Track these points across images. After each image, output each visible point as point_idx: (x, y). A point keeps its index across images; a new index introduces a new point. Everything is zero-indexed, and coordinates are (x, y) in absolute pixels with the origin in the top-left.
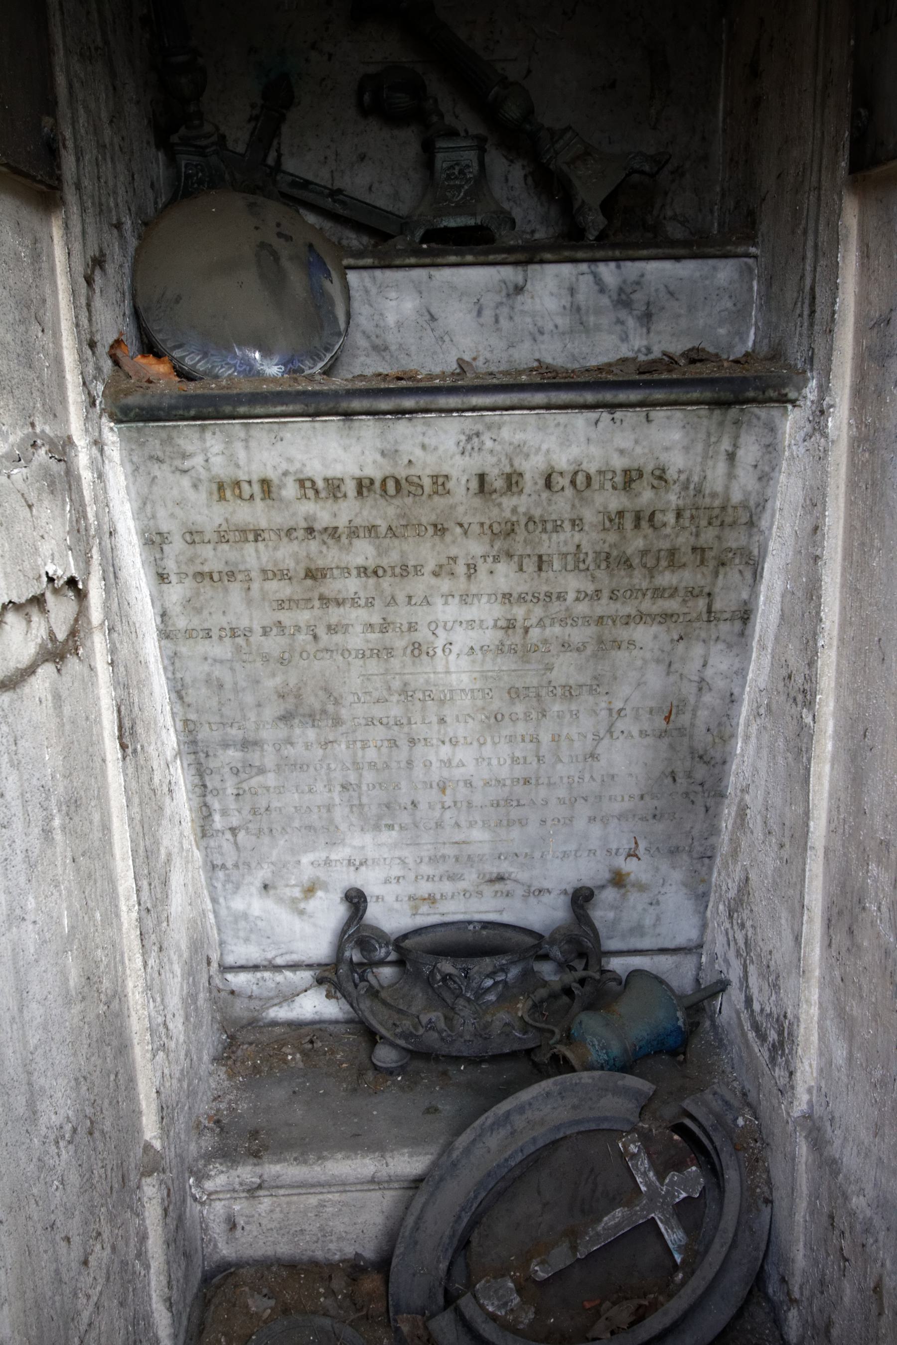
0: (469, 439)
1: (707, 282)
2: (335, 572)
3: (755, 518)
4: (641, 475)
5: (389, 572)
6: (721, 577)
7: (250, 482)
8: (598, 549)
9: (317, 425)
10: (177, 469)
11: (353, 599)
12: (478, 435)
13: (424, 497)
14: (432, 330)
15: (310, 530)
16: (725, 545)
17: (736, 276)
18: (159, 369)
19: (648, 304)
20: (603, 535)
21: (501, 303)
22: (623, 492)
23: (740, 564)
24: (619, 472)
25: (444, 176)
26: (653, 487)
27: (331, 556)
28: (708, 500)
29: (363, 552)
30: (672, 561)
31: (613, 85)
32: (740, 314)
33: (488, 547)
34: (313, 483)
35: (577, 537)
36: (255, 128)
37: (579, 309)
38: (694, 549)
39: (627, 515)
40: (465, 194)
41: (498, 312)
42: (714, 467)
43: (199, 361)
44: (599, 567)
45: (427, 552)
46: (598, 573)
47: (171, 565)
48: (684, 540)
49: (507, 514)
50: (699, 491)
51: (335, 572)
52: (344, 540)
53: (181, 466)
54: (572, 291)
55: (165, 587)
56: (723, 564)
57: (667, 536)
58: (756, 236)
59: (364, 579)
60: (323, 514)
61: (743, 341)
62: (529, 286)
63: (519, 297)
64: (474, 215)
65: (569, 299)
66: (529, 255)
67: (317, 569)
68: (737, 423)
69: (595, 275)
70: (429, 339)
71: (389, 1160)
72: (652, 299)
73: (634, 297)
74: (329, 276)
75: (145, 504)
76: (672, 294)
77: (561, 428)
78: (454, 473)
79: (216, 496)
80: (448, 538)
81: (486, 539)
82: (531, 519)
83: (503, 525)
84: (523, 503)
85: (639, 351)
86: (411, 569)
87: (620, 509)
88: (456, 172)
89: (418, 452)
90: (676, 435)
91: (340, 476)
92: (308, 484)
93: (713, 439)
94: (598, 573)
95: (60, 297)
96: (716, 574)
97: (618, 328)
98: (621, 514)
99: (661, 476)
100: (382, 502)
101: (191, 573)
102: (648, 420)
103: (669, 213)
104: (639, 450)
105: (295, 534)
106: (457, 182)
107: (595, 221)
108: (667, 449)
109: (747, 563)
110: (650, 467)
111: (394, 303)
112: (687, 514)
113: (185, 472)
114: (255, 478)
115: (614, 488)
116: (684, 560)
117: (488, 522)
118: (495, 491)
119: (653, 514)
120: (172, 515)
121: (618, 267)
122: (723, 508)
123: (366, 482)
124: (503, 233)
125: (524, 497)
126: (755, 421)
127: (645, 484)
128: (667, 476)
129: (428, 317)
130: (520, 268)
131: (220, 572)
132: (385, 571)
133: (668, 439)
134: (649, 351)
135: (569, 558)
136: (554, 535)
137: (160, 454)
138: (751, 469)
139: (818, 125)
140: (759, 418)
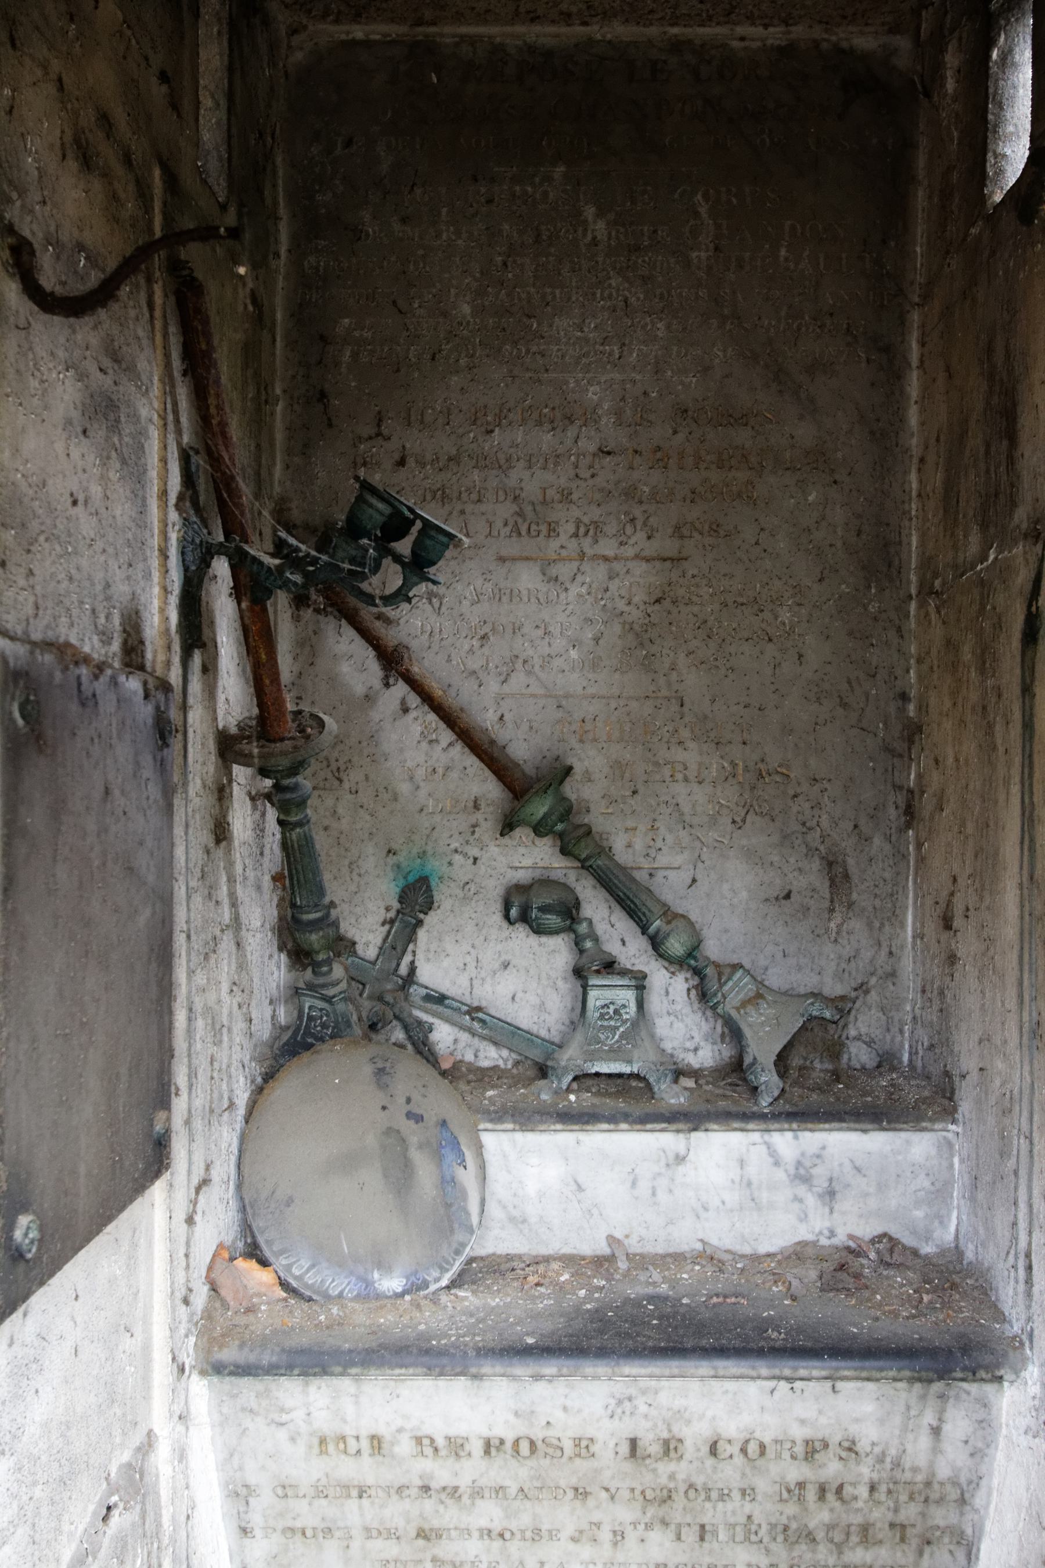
0: (620, 1402)
1: (900, 1158)
2: (453, 1533)
3: (967, 1496)
5: (518, 1536)
6: (926, 1556)
7: (357, 1438)
8: (773, 1521)
10: (273, 1421)
11: (473, 1562)
13: (565, 1459)
14: (579, 1202)
15: (426, 1489)
18: (258, 1278)
19: (831, 1180)
20: (780, 1507)
21: (659, 1174)
22: (804, 1463)
23: (951, 1543)
24: (799, 1442)
25: (597, 1015)
26: (841, 1458)
27: (449, 1516)
28: (908, 1476)
29: (489, 1513)
30: (866, 1536)
31: (788, 896)
33: (639, 1513)
34: (432, 1440)
35: (748, 1508)
36: (389, 932)
37: (749, 1184)
38: (892, 1525)
39: (809, 1486)
40: (621, 1037)
42: (915, 1440)
43: (308, 1270)
44: (775, 1539)
45: (566, 1517)
46: (773, 1546)
47: (256, 1519)
48: (880, 1515)
49: (663, 1480)
50: (897, 1464)
51: (453, 1533)
52: (465, 1499)
53: (277, 1419)
55: (247, 1542)
56: (929, 1543)
57: (858, 1510)
58: (955, 1110)
59: (487, 1542)
60: (442, 1472)
63: (680, 1168)
64: (629, 1062)
66: (690, 1119)
67: (431, 1530)
71: (491, 809)
72: (835, 1175)
74: (461, 1155)
75: (232, 1455)
76: (858, 1170)
78: (600, 1436)
79: (316, 1450)
80: (591, 1502)
81: (638, 1505)
82: (691, 1486)
83: (658, 1492)
84: (683, 1470)
85: (821, 1233)
86: (545, 1534)
87: (801, 1479)
88: (611, 1011)
90: (869, 1408)
91: (465, 1435)
92: (426, 1442)
93: (913, 1413)
94: (773, 1546)
95: (156, 1266)
96: (921, 1553)
97: (796, 1206)
98: (801, 1485)
99: (851, 1448)
100: (513, 1462)
101: (280, 1527)
103: (853, 1033)
104: (823, 1420)
105: (407, 1492)
106: (612, 1023)
107: (768, 1079)
109: (958, 1543)
110: (837, 1438)
112: (883, 1488)
113: (282, 1424)
114: (364, 1433)
115: (793, 1457)
116: (880, 1536)
117: (639, 1488)
118: (649, 1456)
120: (263, 1467)
121: (796, 1138)
122: (928, 1484)
123: (495, 1442)
124: (663, 1087)
125: (683, 1464)
126: (964, 1396)
127: (831, 1455)
128: (858, 1448)
129: (575, 1187)
130: (681, 1136)
131: (314, 1529)
132: (513, 1534)
133: (861, 1410)
134: (832, 1234)
135: (738, 1529)
136: (720, 1505)
137: (255, 1406)
138: (961, 1445)
139: (1027, 1068)
140: (968, 1393)
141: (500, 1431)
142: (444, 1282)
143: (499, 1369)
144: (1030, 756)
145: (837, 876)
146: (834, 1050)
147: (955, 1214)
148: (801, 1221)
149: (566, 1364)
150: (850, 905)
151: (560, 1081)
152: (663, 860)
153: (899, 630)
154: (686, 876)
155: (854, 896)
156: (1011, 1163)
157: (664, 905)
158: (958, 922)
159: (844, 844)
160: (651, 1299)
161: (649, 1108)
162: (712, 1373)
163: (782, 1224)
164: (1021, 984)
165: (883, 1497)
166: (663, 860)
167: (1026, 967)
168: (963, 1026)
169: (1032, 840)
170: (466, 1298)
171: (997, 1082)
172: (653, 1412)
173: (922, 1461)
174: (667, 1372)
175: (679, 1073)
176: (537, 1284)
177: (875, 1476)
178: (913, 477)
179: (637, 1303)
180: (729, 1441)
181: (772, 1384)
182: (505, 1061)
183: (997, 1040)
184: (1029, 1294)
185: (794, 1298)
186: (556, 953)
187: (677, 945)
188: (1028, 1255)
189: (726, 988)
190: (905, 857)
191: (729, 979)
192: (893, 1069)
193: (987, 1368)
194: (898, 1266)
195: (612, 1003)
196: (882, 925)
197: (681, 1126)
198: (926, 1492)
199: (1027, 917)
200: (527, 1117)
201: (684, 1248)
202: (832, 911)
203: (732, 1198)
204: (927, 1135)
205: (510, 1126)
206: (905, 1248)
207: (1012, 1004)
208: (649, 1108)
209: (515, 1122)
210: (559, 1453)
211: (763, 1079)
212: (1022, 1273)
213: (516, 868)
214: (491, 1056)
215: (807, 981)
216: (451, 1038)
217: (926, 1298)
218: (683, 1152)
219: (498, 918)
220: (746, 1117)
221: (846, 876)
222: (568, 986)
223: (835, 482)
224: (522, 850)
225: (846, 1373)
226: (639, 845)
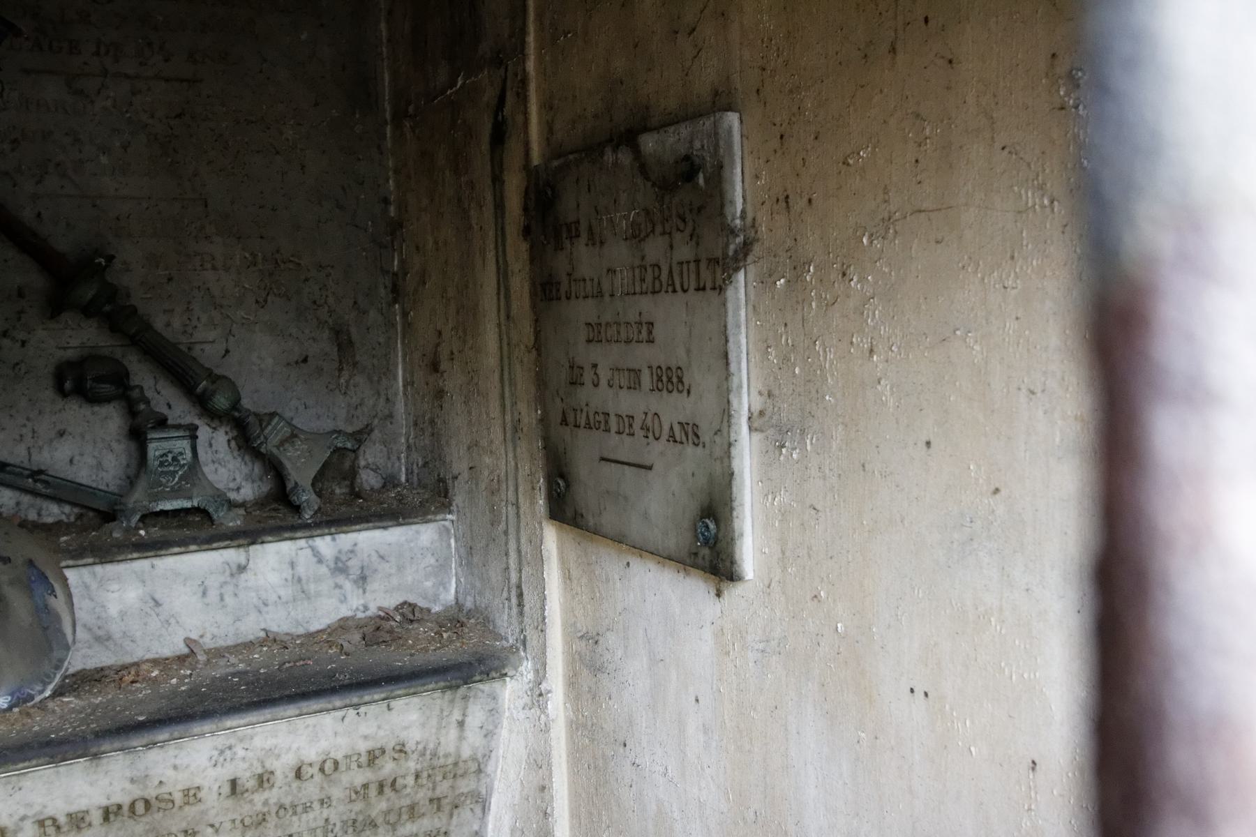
0: (222, 752)
4: (384, 752)
8: (345, 818)
9: (61, 769)
12: (230, 748)
16: (457, 792)
17: (436, 537)
19: (362, 568)
20: (350, 806)
21: (225, 583)
24: (363, 754)
25: (157, 463)
28: (442, 761)
31: (305, 360)
32: (442, 567)
34: (54, 820)
35: (326, 813)
37: (300, 580)
38: (431, 800)
40: (181, 479)
41: (223, 591)
49: (259, 807)
50: (434, 755)
54: (292, 565)
57: (408, 795)
58: (451, 504)
61: (446, 589)
62: (251, 565)
64: (190, 498)
65: (290, 572)
66: (250, 536)
68: (465, 698)
69: (312, 548)
70: (154, 623)
73: (350, 563)
76: (382, 557)
77: (311, 729)
82: (282, 807)
84: (273, 795)
85: (357, 609)
89: (170, 773)
92: (49, 823)
93: (445, 713)
96: (451, 815)
97: (337, 591)
98: (366, 786)
99: (401, 750)
100: (131, 822)
102: (389, 708)
104: (381, 733)
106: (172, 468)
107: (307, 497)
108: (406, 728)
111: (116, 595)
112: (425, 774)
115: (359, 766)
117: (239, 818)
119: (395, 780)
121: (334, 540)
122: (456, 764)
125: (275, 790)
126: (480, 694)
128: (407, 749)
129: (152, 604)
130: (241, 550)
134: (366, 608)
135: (318, 831)
138: (478, 730)
139: (511, 455)
141: (118, 798)
142: (48, 693)
143: (117, 745)
144: (503, 229)
145: (343, 343)
146: (353, 474)
147: (454, 580)
148: (342, 602)
149: (177, 730)
150: (355, 364)
151: (129, 521)
152: (198, 336)
153: (379, 147)
154: (220, 347)
155: (358, 358)
156: (502, 526)
157: (208, 369)
158: (444, 366)
159: (347, 317)
160: (234, 675)
161: (212, 531)
162: (297, 712)
163: (330, 606)
164: (502, 397)
165: (425, 781)
166: (198, 336)
167: (507, 383)
168: (453, 442)
169: (507, 290)
170: (70, 702)
171: (486, 473)
172: (250, 754)
173: (452, 749)
174: (262, 719)
175: (232, 505)
176: (133, 682)
177: (419, 767)
178: (383, 26)
179: (224, 679)
180: (311, 765)
181: (340, 714)
182: (68, 516)
183: (484, 443)
184: (521, 613)
185: (347, 654)
186: (111, 420)
187: (222, 400)
188: (519, 587)
189: (267, 431)
190: (394, 325)
191: (269, 424)
192: (395, 486)
193: (496, 670)
194: (418, 621)
195: (170, 452)
196: (380, 378)
197: (241, 541)
198: (455, 770)
199: (505, 348)
200: (106, 553)
201: (251, 637)
202: (341, 370)
203: (286, 593)
204: (432, 526)
205: (90, 560)
206: (422, 609)
207: (495, 411)
208: (212, 531)
209: (94, 556)
210: (170, 805)
211: (304, 498)
212: (514, 601)
213: (65, 349)
214: (53, 512)
215: (328, 425)
216: (12, 503)
217: (445, 635)
218: (243, 562)
219: (49, 394)
220: (294, 528)
221: (351, 343)
222: (122, 446)
223: (322, 25)
224: (69, 332)
225: (399, 692)
226: (177, 323)
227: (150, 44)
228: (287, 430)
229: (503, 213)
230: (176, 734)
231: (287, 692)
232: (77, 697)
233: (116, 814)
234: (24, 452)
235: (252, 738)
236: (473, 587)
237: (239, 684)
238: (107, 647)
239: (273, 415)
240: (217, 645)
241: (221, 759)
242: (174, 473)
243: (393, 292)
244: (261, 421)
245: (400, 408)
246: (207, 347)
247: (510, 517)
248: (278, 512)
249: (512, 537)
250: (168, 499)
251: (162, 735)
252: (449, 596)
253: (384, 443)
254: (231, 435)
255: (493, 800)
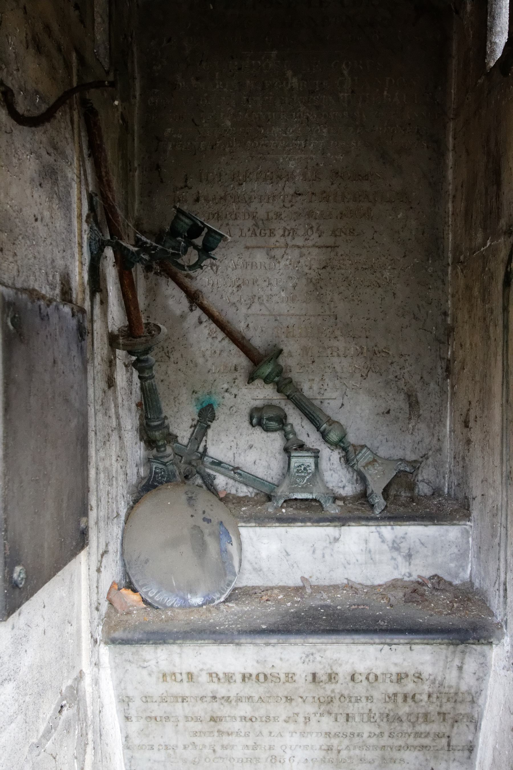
0: (307, 656)
16: (457, 712)
17: (459, 535)
19: (409, 549)
20: (385, 705)
21: (326, 547)
24: (394, 674)
28: (447, 690)
31: (388, 412)
34: (217, 675)
35: (369, 705)
37: (370, 551)
38: (439, 713)
49: (329, 693)
50: (441, 684)
58: (470, 515)
62: (342, 538)
64: (312, 493)
66: (341, 520)
68: (463, 652)
73: (401, 545)
76: (422, 544)
77: (361, 652)
84: (338, 688)
85: (405, 575)
89: (278, 661)
92: (214, 675)
93: (449, 660)
96: (453, 726)
97: (393, 562)
98: (395, 695)
99: (419, 677)
100: (256, 685)
104: (406, 664)
106: (303, 474)
107: (379, 501)
112: (435, 696)
115: (391, 681)
117: (317, 697)
119: (414, 695)
121: (393, 529)
122: (456, 694)
125: (338, 685)
126: (474, 651)
128: (423, 677)
129: (285, 554)
134: (410, 575)
138: (472, 675)
139: (505, 493)
142: (222, 599)
143: (249, 640)
145: (413, 403)
146: (411, 487)
147: (470, 565)
149: (282, 638)
150: (419, 416)
151: (277, 502)
152: (327, 395)
153: (443, 281)
155: (421, 412)
156: (497, 540)
157: (328, 417)
160: (322, 607)
161: (321, 515)
162: (352, 641)
165: (434, 700)
166: (327, 395)
167: (505, 445)
168: (474, 474)
169: (508, 383)
171: (491, 501)
174: (330, 641)
175: (335, 498)
176: (267, 600)
177: (431, 690)
178: (450, 205)
179: (316, 609)
180: (360, 674)
181: (381, 646)
182: (251, 493)
183: (490, 481)
184: (505, 603)
185: (392, 606)
186: (275, 441)
187: (334, 436)
188: (505, 584)
189: (358, 457)
190: (446, 392)
192: (440, 496)
193: (485, 638)
196: (435, 426)
197: (337, 524)
198: (456, 697)
200: (262, 520)
201: (339, 582)
202: (410, 419)
203: (362, 558)
204: (456, 528)
205: (254, 524)
206: (445, 581)
208: (321, 515)
209: (256, 523)
210: (278, 680)
211: (376, 501)
212: (502, 592)
213: (256, 399)
214: (244, 491)
215: (398, 453)
216: (224, 483)
217: (455, 605)
218: (337, 536)
219: (247, 424)
220: (368, 519)
221: (417, 402)
222: (281, 457)
223: (411, 208)
225: (417, 641)
227: (311, 228)
228: (370, 457)
229: (508, 332)
230: (281, 641)
231: (348, 627)
232: (237, 604)
233: (249, 679)
234: (231, 456)
235: (325, 651)
236: (480, 574)
237: (323, 615)
238: (259, 575)
239: (363, 447)
240: (319, 584)
241: (307, 660)
242: (304, 477)
243: (446, 371)
244: (355, 450)
245: (447, 445)
246: (332, 402)
247: (502, 535)
248: (359, 508)
249: (503, 548)
250: (298, 492)
251: (273, 640)
252: (466, 575)
253: (435, 466)
254: (342, 455)
255: (483, 723)
